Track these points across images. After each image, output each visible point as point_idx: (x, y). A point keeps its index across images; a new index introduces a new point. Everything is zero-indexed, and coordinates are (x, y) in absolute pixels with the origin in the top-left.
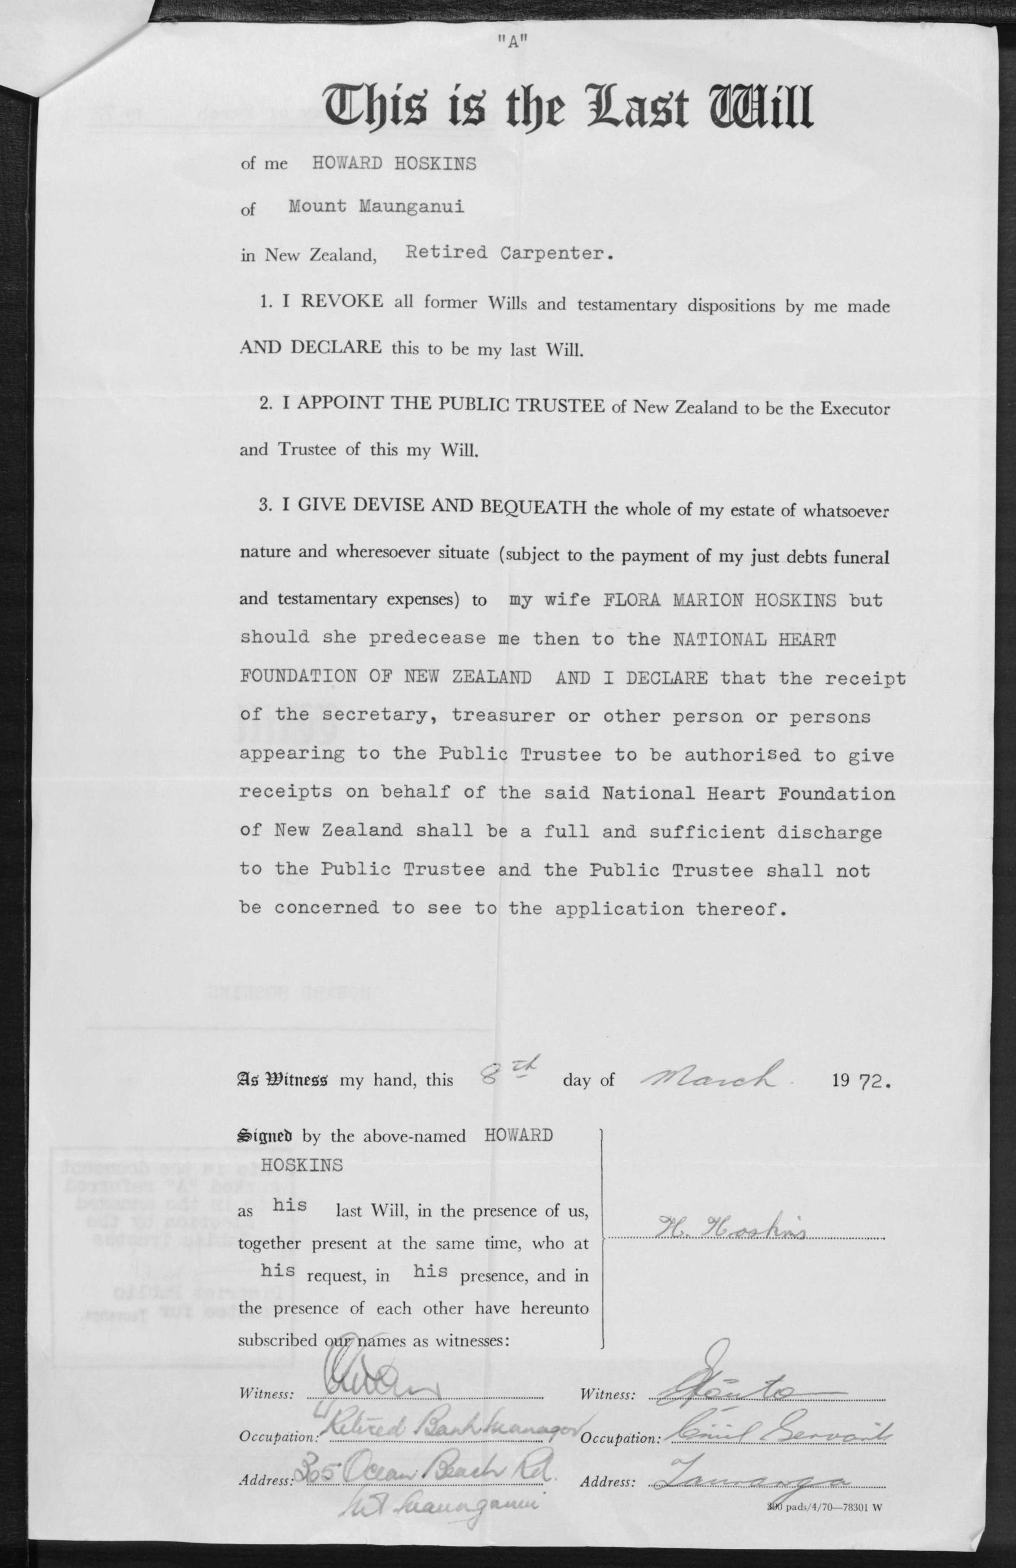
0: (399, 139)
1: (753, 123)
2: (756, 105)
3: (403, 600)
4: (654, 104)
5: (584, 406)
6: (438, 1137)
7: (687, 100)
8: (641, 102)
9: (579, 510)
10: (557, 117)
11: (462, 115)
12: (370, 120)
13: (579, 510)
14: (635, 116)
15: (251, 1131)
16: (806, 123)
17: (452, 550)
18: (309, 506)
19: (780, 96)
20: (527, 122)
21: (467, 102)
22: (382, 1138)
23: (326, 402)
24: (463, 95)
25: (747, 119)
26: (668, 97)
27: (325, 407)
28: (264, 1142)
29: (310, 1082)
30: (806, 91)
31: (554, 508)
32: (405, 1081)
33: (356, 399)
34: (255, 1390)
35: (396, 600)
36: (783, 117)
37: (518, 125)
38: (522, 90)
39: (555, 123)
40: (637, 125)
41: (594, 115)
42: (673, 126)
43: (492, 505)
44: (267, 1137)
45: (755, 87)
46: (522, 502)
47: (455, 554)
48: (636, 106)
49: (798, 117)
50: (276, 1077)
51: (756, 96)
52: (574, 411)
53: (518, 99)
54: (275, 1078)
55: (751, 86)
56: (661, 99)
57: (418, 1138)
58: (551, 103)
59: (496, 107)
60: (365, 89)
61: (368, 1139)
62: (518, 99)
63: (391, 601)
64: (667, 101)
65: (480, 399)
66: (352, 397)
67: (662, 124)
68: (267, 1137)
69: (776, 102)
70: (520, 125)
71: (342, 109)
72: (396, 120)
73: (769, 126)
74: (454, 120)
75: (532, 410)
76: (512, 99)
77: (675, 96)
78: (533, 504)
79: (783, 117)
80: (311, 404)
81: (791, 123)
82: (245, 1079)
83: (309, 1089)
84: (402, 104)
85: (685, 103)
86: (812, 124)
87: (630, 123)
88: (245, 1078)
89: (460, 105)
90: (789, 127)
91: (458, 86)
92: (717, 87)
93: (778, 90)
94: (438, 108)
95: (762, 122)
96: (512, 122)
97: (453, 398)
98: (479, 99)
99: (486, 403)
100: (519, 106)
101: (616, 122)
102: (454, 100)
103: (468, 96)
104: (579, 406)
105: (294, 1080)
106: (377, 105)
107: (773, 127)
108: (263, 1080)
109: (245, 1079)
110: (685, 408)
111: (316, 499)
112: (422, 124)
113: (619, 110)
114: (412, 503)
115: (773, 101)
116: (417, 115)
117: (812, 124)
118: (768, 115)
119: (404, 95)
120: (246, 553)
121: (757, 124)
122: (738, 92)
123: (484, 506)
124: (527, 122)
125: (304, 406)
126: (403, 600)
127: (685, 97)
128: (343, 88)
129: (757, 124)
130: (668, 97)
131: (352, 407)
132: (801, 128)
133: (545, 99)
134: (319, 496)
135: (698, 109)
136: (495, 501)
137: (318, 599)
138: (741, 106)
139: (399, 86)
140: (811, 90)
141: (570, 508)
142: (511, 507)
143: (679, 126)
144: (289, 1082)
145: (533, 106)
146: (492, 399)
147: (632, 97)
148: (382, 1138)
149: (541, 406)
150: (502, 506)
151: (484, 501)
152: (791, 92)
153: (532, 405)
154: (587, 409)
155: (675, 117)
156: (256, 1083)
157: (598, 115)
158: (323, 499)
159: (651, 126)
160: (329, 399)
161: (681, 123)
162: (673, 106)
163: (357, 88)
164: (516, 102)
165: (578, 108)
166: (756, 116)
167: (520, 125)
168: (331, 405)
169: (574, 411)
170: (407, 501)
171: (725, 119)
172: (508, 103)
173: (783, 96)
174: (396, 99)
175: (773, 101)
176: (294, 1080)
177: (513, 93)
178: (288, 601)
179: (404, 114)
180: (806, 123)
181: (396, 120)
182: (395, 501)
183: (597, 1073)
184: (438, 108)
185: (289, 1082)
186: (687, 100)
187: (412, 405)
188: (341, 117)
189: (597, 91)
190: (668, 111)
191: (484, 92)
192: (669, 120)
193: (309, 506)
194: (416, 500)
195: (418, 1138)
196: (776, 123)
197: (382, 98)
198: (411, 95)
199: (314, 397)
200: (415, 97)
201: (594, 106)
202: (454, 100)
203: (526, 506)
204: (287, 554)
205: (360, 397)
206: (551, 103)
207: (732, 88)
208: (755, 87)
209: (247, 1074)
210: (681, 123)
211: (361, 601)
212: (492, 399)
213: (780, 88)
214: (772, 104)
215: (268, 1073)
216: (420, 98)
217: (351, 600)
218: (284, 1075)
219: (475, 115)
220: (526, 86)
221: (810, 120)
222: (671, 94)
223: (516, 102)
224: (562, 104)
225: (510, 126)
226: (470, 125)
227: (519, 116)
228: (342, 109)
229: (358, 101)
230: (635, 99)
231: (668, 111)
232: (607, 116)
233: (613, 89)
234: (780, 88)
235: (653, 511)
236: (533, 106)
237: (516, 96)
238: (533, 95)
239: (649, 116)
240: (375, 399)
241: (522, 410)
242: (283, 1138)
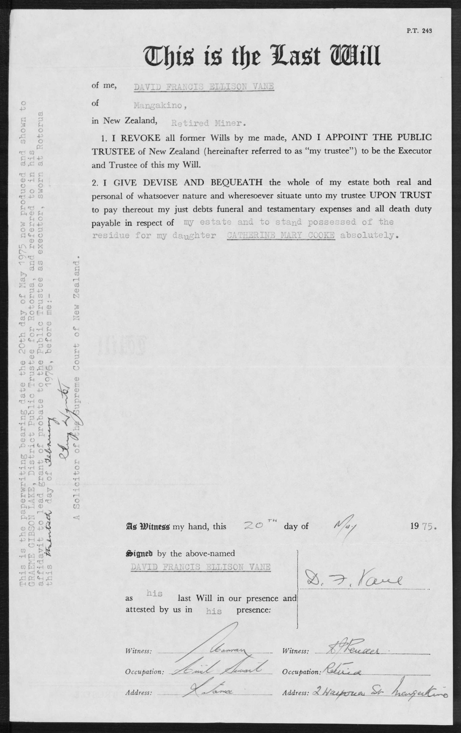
1: (351, 63)
2: (353, 55)
3: (328, 209)
4: (304, 54)
5: (125, 151)
7: (319, 52)
8: (297, 53)
9: (259, 183)
10: (257, 61)
11: (211, 60)
12: (166, 63)
13: (259, 183)
14: (294, 60)
16: (377, 63)
17: (284, 195)
19: (364, 50)
20: (242, 63)
21: (185, 54)
24: (211, 51)
25: (348, 61)
26: (311, 50)
29: (161, 528)
30: (377, 48)
31: (246, 183)
35: (325, 209)
36: (366, 60)
37: (238, 65)
38: (240, 48)
39: (256, 64)
40: (295, 64)
41: (275, 60)
43: (216, 182)
45: (352, 46)
46: (231, 180)
47: (285, 196)
49: (373, 60)
50: (145, 525)
51: (353, 50)
52: (120, 154)
53: (238, 52)
54: (144, 526)
56: (307, 52)
58: (254, 54)
59: (227, 56)
60: (163, 49)
62: (238, 52)
63: (322, 210)
64: (309, 53)
67: (308, 64)
68: (141, 554)
69: (363, 53)
71: (153, 58)
72: (179, 63)
73: (359, 64)
74: (207, 63)
75: (100, 154)
76: (235, 52)
77: (314, 50)
78: (237, 181)
79: (366, 60)
81: (370, 63)
82: (130, 526)
83: (161, 531)
84: (182, 56)
85: (319, 54)
86: (380, 63)
87: (292, 63)
88: (130, 526)
90: (369, 65)
91: (208, 46)
92: (334, 46)
94: (199, 57)
95: (356, 63)
96: (235, 63)
98: (191, 53)
100: (238, 56)
101: (285, 63)
102: (207, 53)
104: (122, 152)
107: (361, 65)
108: (139, 527)
109: (130, 526)
110: (174, 152)
111: (122, 180)
112: (192, 65)
113: (286, 57)
115: (361, 53)
116: (189, 61)
117: (380, 63)
118: (359, 59)
119: (183, 51)
120: (185, 196)
122: (344, 48)
123: (212, 182)
124: (242, 63)
126: (328, 209)
127: (318, 50)
128: (153, 48)
129: (353, 63)
130: (311, 50)
132: (374, 65)
133: (251, 52)
134: (124, 179)
136: (218, 180)
137: (286, 209)
138: (344, 55)
139: (180, 47)
140: (379, 48)
141: (254, 182)
142: (226, 182)
143: (315, 65)
145: (245, 56)
149: (104, 152)
150: (221, 182)
151: (212, 180)
152: (370, 48)
153: (100, 152)
154: (126, 153)
155: (313, 60)
156: (135, 528)
158: (126, 180)
161: (317, 63)
162: (313, 55)
163: (160, 48)
165: (267, 56)
166: (353, 59)
167: (239, 65)
169: (120, 154)
170: (169, 181)
171: (338, 61)
172: (205, 54)
173: (366, 50)
174: (179, 53)
175: (361, 53)
177: (235, 49)
178: (272, 210)
179: (182, 60)
180: (377, 63)
181: (179, 63)
182: (163, 181)
184: (199, 57)
186: (319, 52)
188: (153, 62)
189: (276, 48)
190: (309, 58)
191: (193, 49)
194: (173, 180)
195: (212, 554)
196: (363, 63)
197: (172, 53)
198: (305, 51)
200: (188, 52)
201: (275, 56)
202: (207, 53)
203: (233, 182)
204: (205, 197)
206: (254, 54)
208: (352, 46)
209: (131, 524)
210: (317, 63)
211: (307, 210)
213: (364, 46)
214: (360, 54)
215: (141, 523)
216: (218, 53)
217: (303, 210)
219: (217, 61)
220: (242, 46)
221: (319, 62)
222: (312, 49)
223: (237, 54)
224: (259, 55)
226: (186, 66)
227: (238, 60)
228: (153, 58)
229: (161, 54)
230: (294, 52)
231: (309, 58)
232: (281, 60)
234: (364, 46)
235: (301, 183)
236: (245, 56)
237: (237, 51)
238: (245, 51)
239: (301, 60)
241: (95, 154)
242: (148, 554)
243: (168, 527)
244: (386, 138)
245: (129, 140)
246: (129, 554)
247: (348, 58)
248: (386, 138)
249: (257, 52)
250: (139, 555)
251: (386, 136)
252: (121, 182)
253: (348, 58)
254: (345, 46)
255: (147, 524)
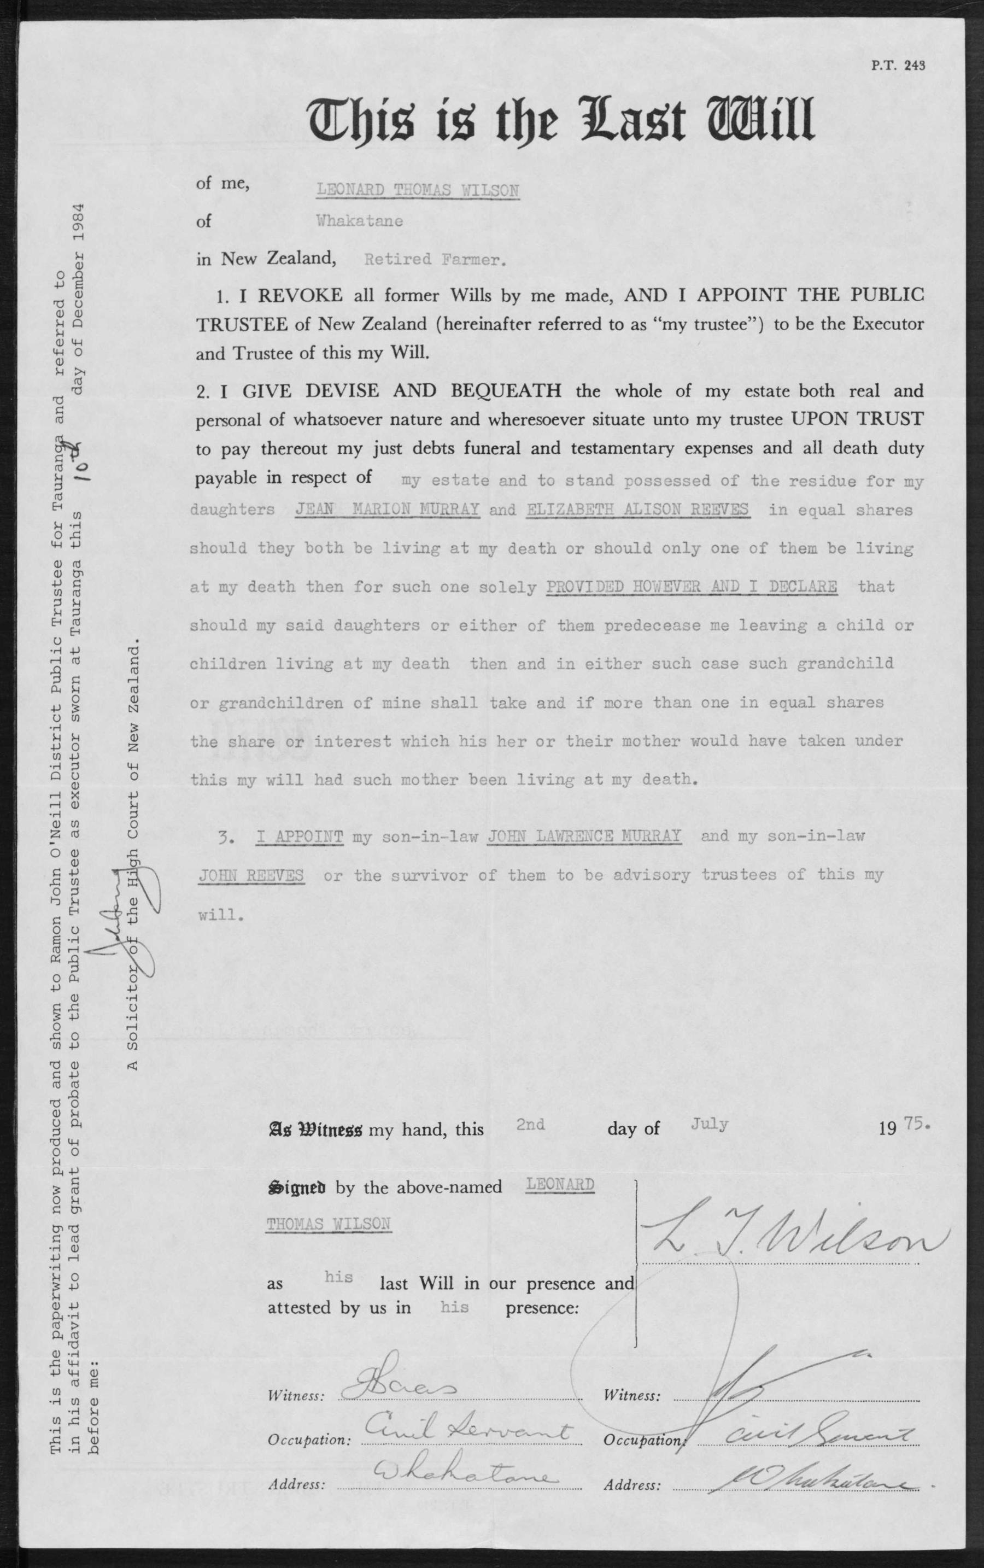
0: (385, 156)
1: (752, 135)
2: (755, 117)
4: (650, 117)
6: (474, 1188)
7: (684, 112)
8: (636, 114)
10: (550, 131)
11: (451, 129)
12: (356, 136)
14: (630, 129)
15: (283, 1183)
16: (808, 135)
18: (254, 394)
19: (780, 107)
20: (518, 136)
22: (416, 1189)
23: (727, 295)
24: (451, 109)
25: (746, 131)
27: (727, 300)
28: (296, 1194)
29: (344, 1132)
30: (807, 103)
32: (438, 1131)
33: (758, 292)
34: (620, 1392)
36: (784, 129)
39: (548, 137)
40: (632, 138)
42: (670, 139)
44: (300, 1188)
45: (754, 99)
48: (631, 118)
49: (799, 128)
50: (309, 1128)
51: (755, 107)
53: (508, 112)
54: (307, 1129)
55: (751, 97)
56: (657, 112)
57: (453, 1188)
58: (543, 116)
59: (485, 122)
60: (350, 105)
61: (402, 1190)
62: (508, 112)
64: (662, 113)
65: (893, 289)
66: (754, 289)
67: (659, 137)
68: (300, 1188)
69: (776, 113)
70: (511, 140)
71: (327, 124)
72: (382, 135)
73: (769, 138)
74: (443, 135)
76: (502, 112)
77: (672, 108)
79: (784, 129)
80: (711, 297)
81: (792, 135)
82: (277, 1129)
84: (389, 119)
85: (682, 115)
86: (813, 136)
87: (625, 136)
88: (277, 1128)
89: (449, 119)
92: (714, 99)
93: (778, 103)
94: (425, 122)
95: (761, 134)
97: (866, 289)
99: (900, 293)
100: (510, 120)
101: (610, 136)
102: (442, 113)
103: (456, 110)
105: (328, 1130)
106: (363, 121)
108: (296, 1130)
109: (277, 1129)
113: (613, 123)
114: (367, 389)
117: (813, 136)
119: (391, 109)
121: (756, 136)
122: (737, 104)
124: (518, 136)
125: (704, 299)
127: (682, 108)
128: (327, 103)
129: (756, 136)
130: (664, 109)
131: (754, 299)
132: (802, 140)
133: (537, 112)
135: (696, 121)
138: (737, 119)
139: (385, 100)
140: (812, 103)
143: (675, 140)
144: (322, 1132)
145: (525, 120)
146: (906, 289)
147: (626, 109)
148: (416, 1189)
152: (792, 104)
155: (671, 130)
156: (288, 1132)
157: (592, 128)
159: (646, 139)
160: (730, 292)
161: (678, 136)
162: (669, 118)
164: (507, 116)
165: (571, 122)
166: (755, 128)
168: (732, 298)
173: (784, 108)
174: (382, 114)
176: (328, 1130)
177: (504, 105)
179: (390, 129)
180: (808, 135)
181: (382, 135)
183: (642, 1120)
184: (425, 122)
185: (322, 1132)
186: (684, 112)
187: (820, 297)
188: (326, 133)
190: (663, 124)
192: (665, 133)
193: (254, 394)
195: (453, 1188)
196: (777, 135)
197: (368, 113)
199: (715, 289)
201: (588, 120)
202: (442, 113)
205: (763, 290)
206: (543, 116)
207: (731, 101)
208: (754, 99)
209: (279, 1124)
210: (678, 136)
212: (906, 289)
213: (780, 99)
214: (772, 116)
215: (301, 1123)
218: (317, 1125)
219: (464, 130)
221: (812, 132)
222: (667, 106)
224: (555, 118)
225: (500, 140)
227: (510, 129)
228: (327, 124)
229: (344, 116)
230: (630, 112)
231: (663, 124)
232: (601, 129)
233: (607, 102)
234: (780, 99)
236: (525, 120)
238: (524, 109)
239: (645, 129)
240: (777, 291)
242: (316, 1190)
243: (359, 1132)
244: (827, 297)
245: (276, 301)
246: (275, 1188)
247: (744, 124)
248: (827, 297)
249: (550, 112)
250: (297, 1190)
251: (827, 292)
252: (257, 390)
253: (744, 124)
254: (738, 98)
255: (314, 1124)
